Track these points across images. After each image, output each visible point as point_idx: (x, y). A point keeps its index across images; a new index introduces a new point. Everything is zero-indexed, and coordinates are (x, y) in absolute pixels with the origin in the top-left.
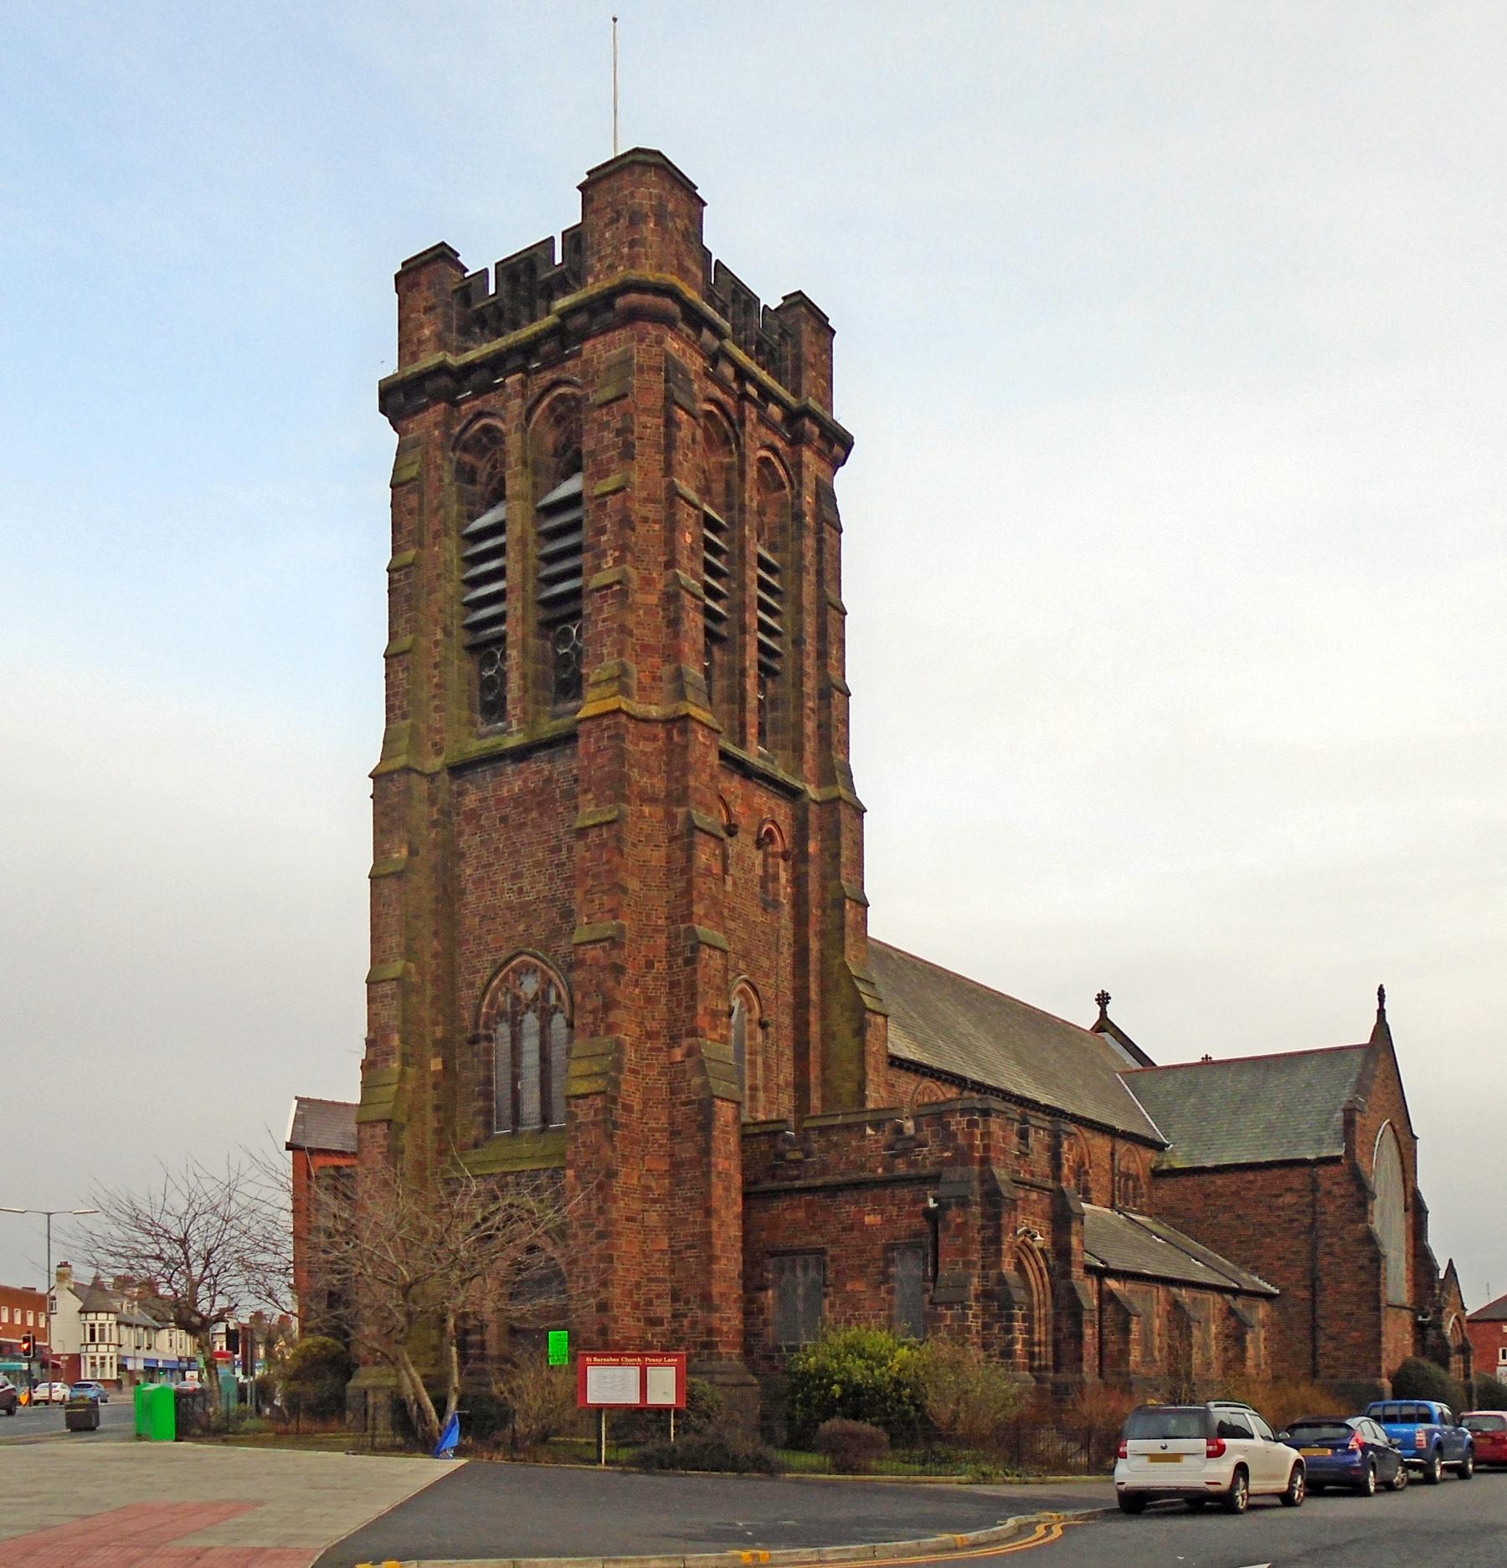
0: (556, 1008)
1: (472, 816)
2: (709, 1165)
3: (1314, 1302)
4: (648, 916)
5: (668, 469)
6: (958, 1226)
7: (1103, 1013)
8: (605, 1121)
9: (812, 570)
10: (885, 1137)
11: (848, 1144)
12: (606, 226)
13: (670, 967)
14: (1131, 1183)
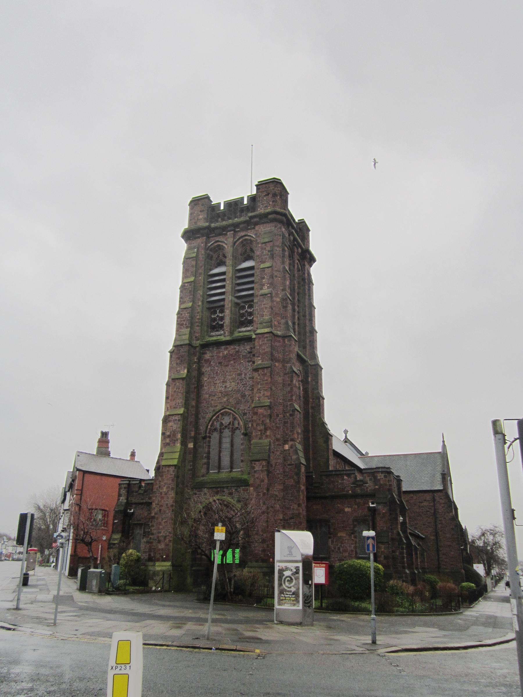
0: (237, 428)
1: (208, 361)
3: (437, 540)
4: (277, 399)
7: (346, 436)
13: (284, 417)
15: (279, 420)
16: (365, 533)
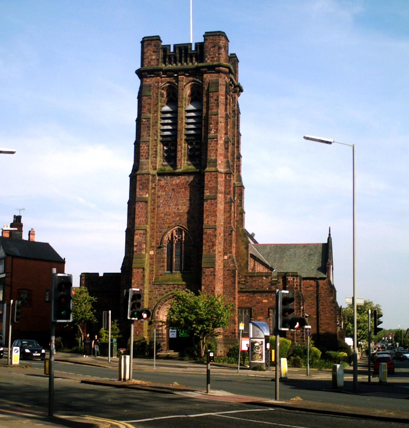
1: (162, 187)
4: (220, 222)
5: (226, 110)
11: (258, 281)
13: (224, 235)
15: (221, 238)
16: (309, 327)
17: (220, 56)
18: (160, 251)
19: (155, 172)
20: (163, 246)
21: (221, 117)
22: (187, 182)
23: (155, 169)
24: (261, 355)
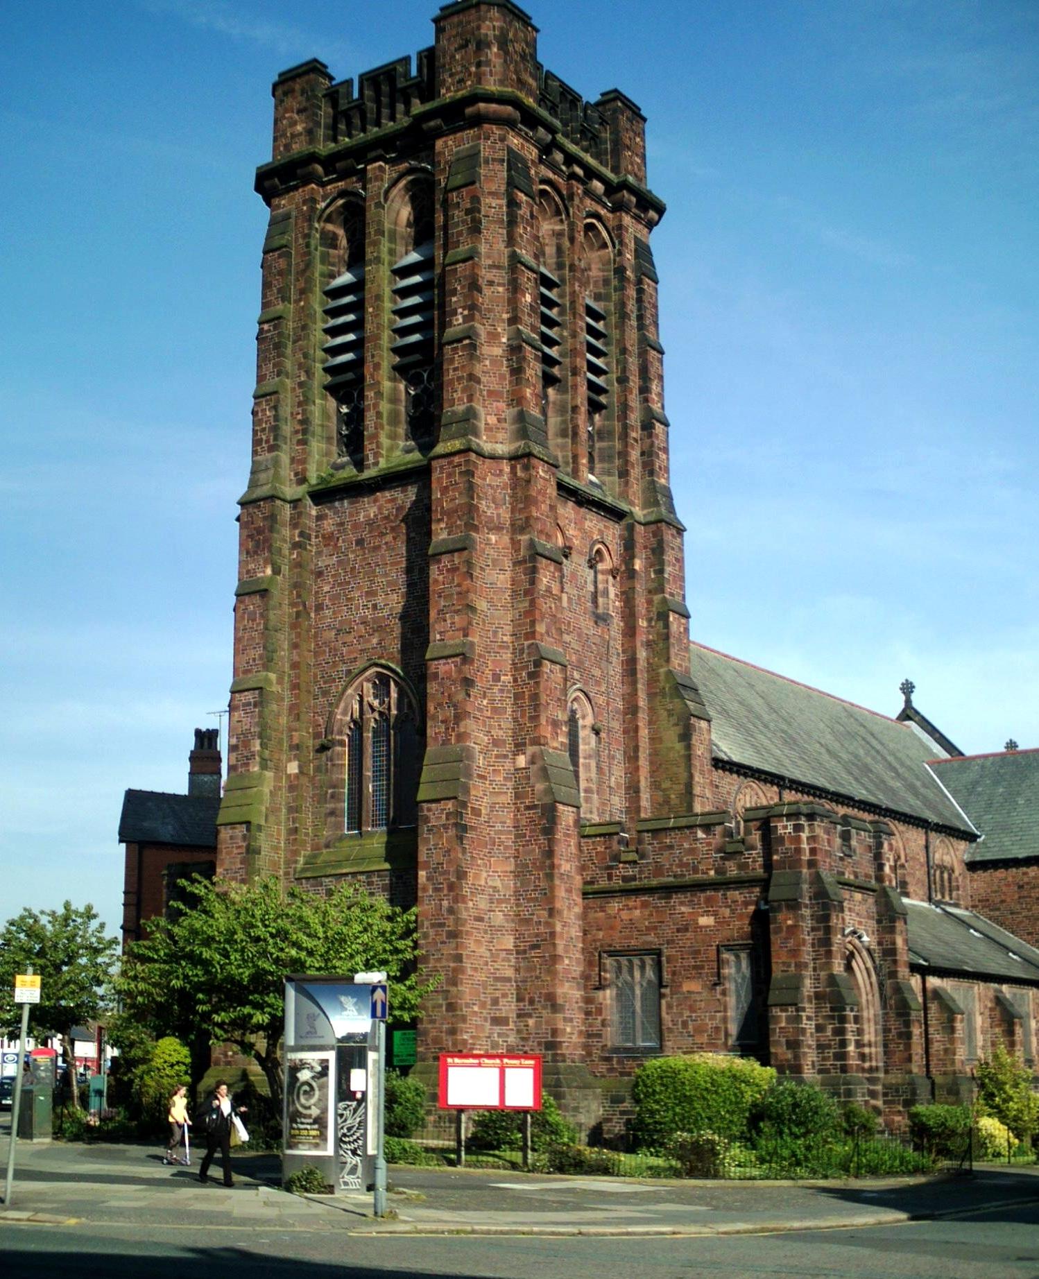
1: (329, 539)
2: (552, 866)
4: (495, 633)
5: (511, 241)
6: (789, 927)
7: (908, 702)
8: (456, 825)
9: (634, 316)
10: (717, 838)
12: (456, 50)
13: (515, 680)
14: (946, 876)
15: (501, 691)
17: (483, 68)
18: (324, 758)
19: (301, 490)
20: (333, 743)
21: (490, 267)
22: (399, 509)
23: (302, 480)
24: (320, 1122)
